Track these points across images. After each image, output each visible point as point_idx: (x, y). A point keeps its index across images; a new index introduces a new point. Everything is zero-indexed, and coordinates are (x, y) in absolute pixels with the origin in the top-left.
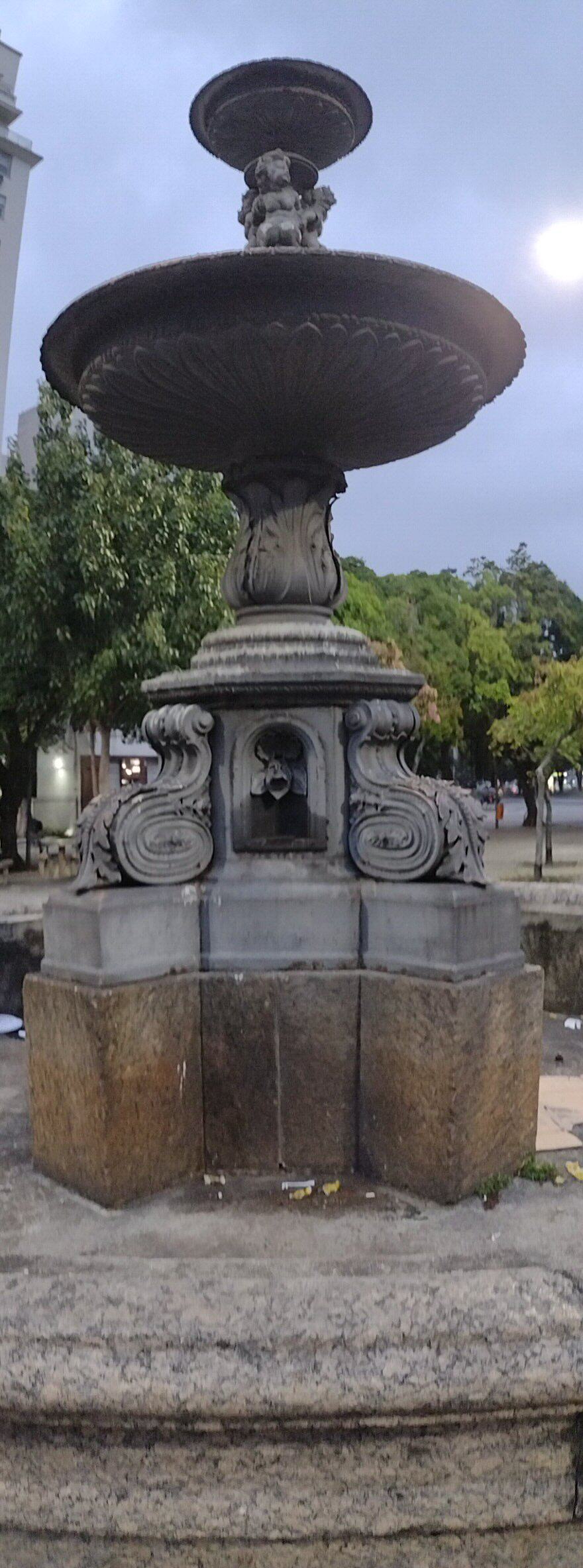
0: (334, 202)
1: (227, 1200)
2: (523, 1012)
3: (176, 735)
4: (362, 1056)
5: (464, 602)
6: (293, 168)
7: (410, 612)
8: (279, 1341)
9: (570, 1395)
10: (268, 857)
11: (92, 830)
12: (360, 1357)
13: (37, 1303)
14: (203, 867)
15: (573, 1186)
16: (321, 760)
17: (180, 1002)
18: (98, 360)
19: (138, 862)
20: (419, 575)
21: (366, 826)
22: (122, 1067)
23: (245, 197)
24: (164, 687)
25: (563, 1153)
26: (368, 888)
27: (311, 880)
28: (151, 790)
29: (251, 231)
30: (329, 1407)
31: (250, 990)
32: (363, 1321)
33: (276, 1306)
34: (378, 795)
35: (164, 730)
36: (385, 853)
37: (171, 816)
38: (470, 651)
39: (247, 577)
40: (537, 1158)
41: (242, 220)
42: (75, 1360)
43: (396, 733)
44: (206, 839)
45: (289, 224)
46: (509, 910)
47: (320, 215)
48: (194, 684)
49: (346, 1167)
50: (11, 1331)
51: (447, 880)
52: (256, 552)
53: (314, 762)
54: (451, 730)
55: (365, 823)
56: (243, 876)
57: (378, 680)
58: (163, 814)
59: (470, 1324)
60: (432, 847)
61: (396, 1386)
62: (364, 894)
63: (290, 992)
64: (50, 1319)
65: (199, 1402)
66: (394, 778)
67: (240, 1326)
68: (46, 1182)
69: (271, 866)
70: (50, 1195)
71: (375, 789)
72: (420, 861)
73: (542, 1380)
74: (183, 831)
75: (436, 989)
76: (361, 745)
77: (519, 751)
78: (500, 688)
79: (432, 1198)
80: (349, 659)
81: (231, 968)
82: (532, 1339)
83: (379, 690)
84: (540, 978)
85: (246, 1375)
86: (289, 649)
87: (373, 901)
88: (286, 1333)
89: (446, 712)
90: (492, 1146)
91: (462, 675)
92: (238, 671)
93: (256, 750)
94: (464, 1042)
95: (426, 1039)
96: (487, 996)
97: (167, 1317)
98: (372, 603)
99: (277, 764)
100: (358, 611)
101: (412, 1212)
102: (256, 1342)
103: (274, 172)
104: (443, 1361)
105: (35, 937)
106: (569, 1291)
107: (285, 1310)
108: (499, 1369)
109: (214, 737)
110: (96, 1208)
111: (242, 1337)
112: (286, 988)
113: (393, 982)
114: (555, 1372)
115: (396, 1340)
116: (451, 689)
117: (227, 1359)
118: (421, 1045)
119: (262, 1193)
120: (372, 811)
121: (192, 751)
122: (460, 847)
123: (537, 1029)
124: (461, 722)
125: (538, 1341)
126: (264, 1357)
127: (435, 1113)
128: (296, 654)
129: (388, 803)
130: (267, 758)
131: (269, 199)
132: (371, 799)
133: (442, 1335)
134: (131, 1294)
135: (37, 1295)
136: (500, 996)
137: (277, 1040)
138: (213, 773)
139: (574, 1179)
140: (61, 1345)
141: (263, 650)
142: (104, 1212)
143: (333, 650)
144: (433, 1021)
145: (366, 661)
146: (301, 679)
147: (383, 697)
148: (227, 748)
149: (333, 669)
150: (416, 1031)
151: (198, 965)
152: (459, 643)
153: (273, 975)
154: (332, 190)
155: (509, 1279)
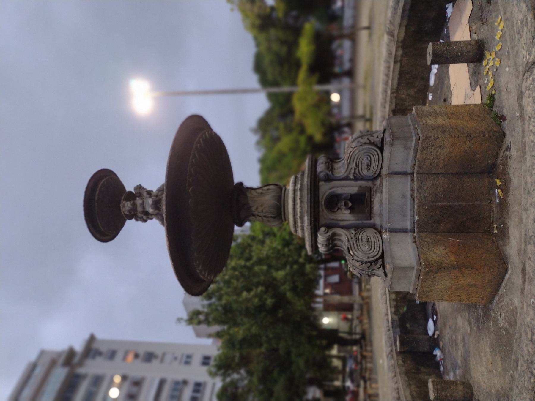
1: (504, 223)
2: (430, 113)
11: (363, 270)
14: (376, 231)
15: (496, 86)
16: (339, 189)
17: (426, 239)
18: (198, 271)
19: (374, 254)
21: (362, 172)
22: (450, 261)
23: (137, 220)
24: (311, 246)
25: (483, 93)
26: (384, 171)
27: (381, 192)
28: (348, 248)
34: (351, 168)
37: (358, 241)
39: (271, 217)
40: (484, 102)
41: (145, 221)
43: (329, 163)
44: (365, 230)
45: (150, 201)
47: (145, 190)
48: (310, 234)
49: (490, 177)
53: (339, 191)
55: (361, 173)
56: (379, 217)
58: (357, 244)
60: (371, 148)
63: (422, 199)
66: (345, 163)
68: (497, 298)
69: (376, 207)
70: (502, 296)
72: (376, 153)
74: (363, 237)
76: (333, 174)
79: (502, 142)
80: (302, 180)
81: (413, 221)
84: (417, 108)
86: (298, 201)
92: (306, 218)
93: (334, 212)
95: (440, 147)
96: (424, 126)
99: (339, 205)
101: (508, 149)
103: (129, 207)
109: (329, 227)
110: (507, 276)
112: (420, 200)
119: (501, 209)
120: (357, 171)
121: (334, 234)
122: (371, 138)
127: (468, 143)
130: (337, 208)
131: (139, 209)
132: (353, 171)
136: (424, 121)
137: (439, 204)
138: (343, 227)
139: (493, 86)
141: (298, 210)
142: (509, 272)
143: (299, 186)
144: (433, 145)
146: (309, 196)
147: (316, 167)
148: (334, 222)
149: (306, 185)
150: (437, 152)
151: (412, 233)
153: (416, 205)
155: (525, 94)
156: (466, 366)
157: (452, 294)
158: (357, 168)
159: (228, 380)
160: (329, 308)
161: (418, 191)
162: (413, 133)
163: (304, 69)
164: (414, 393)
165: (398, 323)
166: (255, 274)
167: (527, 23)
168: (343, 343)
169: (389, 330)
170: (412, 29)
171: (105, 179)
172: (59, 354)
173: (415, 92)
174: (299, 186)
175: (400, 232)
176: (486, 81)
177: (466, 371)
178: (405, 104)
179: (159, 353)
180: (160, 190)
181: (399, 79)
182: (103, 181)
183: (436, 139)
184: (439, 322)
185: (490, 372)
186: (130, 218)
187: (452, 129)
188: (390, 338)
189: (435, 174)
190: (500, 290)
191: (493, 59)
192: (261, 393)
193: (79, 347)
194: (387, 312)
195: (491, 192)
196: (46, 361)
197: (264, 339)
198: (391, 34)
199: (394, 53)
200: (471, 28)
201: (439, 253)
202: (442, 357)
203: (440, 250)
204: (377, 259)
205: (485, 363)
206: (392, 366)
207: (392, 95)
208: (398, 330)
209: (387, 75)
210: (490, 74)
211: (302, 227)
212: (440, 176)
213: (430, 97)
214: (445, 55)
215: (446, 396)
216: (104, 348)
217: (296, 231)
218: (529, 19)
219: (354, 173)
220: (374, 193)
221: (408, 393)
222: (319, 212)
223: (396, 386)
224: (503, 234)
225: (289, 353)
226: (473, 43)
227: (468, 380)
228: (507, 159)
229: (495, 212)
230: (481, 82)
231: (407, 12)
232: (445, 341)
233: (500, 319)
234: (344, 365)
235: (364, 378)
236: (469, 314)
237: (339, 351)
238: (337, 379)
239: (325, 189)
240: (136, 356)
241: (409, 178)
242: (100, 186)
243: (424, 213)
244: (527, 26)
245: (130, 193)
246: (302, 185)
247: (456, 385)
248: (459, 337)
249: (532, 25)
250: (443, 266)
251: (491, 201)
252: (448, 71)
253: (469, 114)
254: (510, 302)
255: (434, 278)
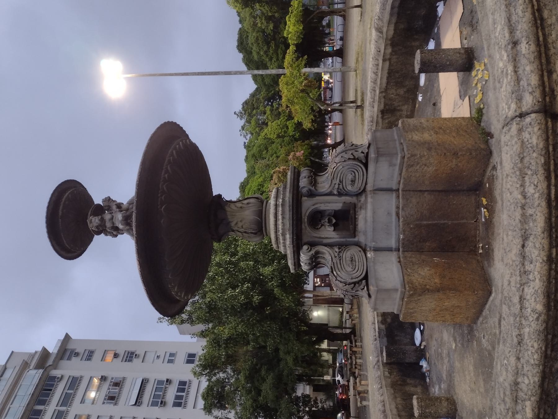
0: (109, 197)
1: (489, 244)
2: (416, 126)
3: (311, 258)
4: (432, 189)
5: (257, 140)
6: (95, 214)
7: (261, 163)
8: (522, 227)
9: (543, 126)
10: (357, 225)
12: (528, 201)
13: (510, 310)
14: (360, 249)
15: (485, 100)
16: (322, 205)
17: (411, 260)
18: (173, 293)
19: (358, 274)
20: (247, 159)
23: (106, 235)
25: (471, 104)
26: (369, 187)
27: (366, 209)
29: (121, 232)
30: (546, 211)
31: (407, 233)
32: (516, 199)
33: (511, 228)
34: (335, 184)
35: (309, 263)
36: (357, 181)
38: (276, 138)
39: (252, 233)
40: (473, 116)
41: (116, 236)
42: (528, 297)
43: (312, 177)
44: (350, 248)
45: (119, 216)
46: (378, 134)
47: (115, 203)
49: (477, 195)
50: (518, 319)
51: (367, 157)
52: (243, 230)
53: (322, 207)
54: (306, 146)
55: (345, 189)
56: (364, 234)
57: (292, 184)
58: (340, 264)
59: (517, 163)
60: (355, 164)
61: (538, 188)
62: (372, 189)
63: (407, 218)
64: (514, 305)
65: (543, 255)
67: (517, 240)
69: (361, 224)
70: (486, 318)
71: (333, 185)
72: (360, 169)
73: (537, 138)
74: (347, 256)
75: (407, 162)
76: (316, 190)
77: (315, 116)
78: (290, 124)
79: (489, 160)
80: (284, 194)
81: (398, 240)
82: (523, 142)
83: (296, 183)
84: (403, 120)
85: (533, 239)
86: (280, 217)
87: (374, 185)
88: (519, 225)
89: (300, 148)
90: (468, 136)
91: (285, 141)
92: (288, 236)
93: (317, 229)
94: (427, 151)
95: (425, 165)
97: (514, 265)
98: (257, 179)
99: (323, 221)
100: (260, 185)
101: (494, 168)
102: (522, 235)
104: (529, 172)
105: (384, 315)
106: (508, 128)
107: (512, 225)
108: (533, 153)
109: (312, 245)
110: (491, 298)
111: (521, 239)
112: (406, 218)
113: (404, 178)
114: (534, 133)
115: (522, 189)
116: (290, 146)
117: (528, 246)
118: (428, 167)
120: (341, 186)
121: (317, 253)
122: (355, 153)
123: (423, 121)
124: (304, 141)
125: (523, 140)
126: (527, 233)
127: (454, 160)
128: (282, 214)
129: (338, 180)
131: (108, 225)
132: (337, 186)
133: (520, 173)
134: (507, 277)
135: (507, 310)
136: (410, 137)
137: (425, 222)
138: (326, 245)
139: (481, 99)
140: (523, 302)
141: (280, 227)
142: (493, 295)
145: (285, 188)
146: (291, 213)
148: (317, 240)
150: (423, 169)
152: (273, 143)
153: (401, 224)
154: (104, 198)
156: (450, 381)
157: (436, 315)
158: (341, 184)
159: (214, 379)
160: (319, 302)
161: (403, 209)
162: (398, 148)
163: (292, 48)
164: (400, 406)
165: (385, 333)
166: (241, 270)
167: (507, 74)
168: (333, 338)
169: (376, 340)
170: (402, 26)
171: (69, 192)
172: (33, 356)
173: (405, 92)
174: (281, 200)
175: (385, 251)
176: (475, 93)
177: (451, 387)
178: (394, 104)
179: (140, 352)
180: (130, 203)
181: (388, 78)
182: (67, 194)
183: (421, 157)
184: (426, 333)
185: (473, 391)
186: (99, 233)
187: (439, 146)
188: (377, 348)
189: (420, 191)
190: (484, 311)
191: (482, 71)
192: (249, 392)
193: (53, 348)
194: (375, 321)
195: (478, 211)
196: (17, 363)
197: (251, 337)
198: (379, 30)
199: (382, 51)
200: (461, 32)
201: (423, 274)
202: (428, 369)
203: (425, 271)
204: (361, 280)
205: (468, 381)
206: (378, 377)
207: (381, 95)
208: (385, 339)
209: (376, 73)
210: (479, 86)
211: (284, 243)
212: (426, 193)
213: (420, 99)
214: (433, 64)
215: (430, 413)
216: (80, 350)
217: (278, 247)
218: (509, 72)
219: (338, 189)
220: (359, 210)
221: (393, 406)
222: (301, 229)
223: (382, 398)
224: (488, 254)
225: (277, 350)
226: (463, 51)
227: (452, 396)
228: (493, 179)
229: (481, 232)
230: (470, 92)
231: (396, 10)
232: (431, 352)
233: (484, 340)
234: (334, 359)
235: (353, 374)
236: (454, 330)
237: (329, 345)
238: (328, 374)
239: (308, 205)
240: (116, 356)
241: (394, 195)
242: (63, 200)
243: (408, 231)
244: (507, 78)
245: (99, 205)
246: (283, 200)
247: (441, 402)
248: (445, 351)
249: (511, 78)
250: (427, 289)
251: (477, 220)
252: (438, 77)
253: (457, 129)
254: (493, 325)
255: (418, 300)
